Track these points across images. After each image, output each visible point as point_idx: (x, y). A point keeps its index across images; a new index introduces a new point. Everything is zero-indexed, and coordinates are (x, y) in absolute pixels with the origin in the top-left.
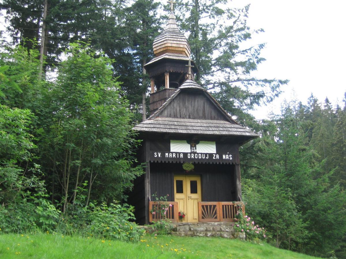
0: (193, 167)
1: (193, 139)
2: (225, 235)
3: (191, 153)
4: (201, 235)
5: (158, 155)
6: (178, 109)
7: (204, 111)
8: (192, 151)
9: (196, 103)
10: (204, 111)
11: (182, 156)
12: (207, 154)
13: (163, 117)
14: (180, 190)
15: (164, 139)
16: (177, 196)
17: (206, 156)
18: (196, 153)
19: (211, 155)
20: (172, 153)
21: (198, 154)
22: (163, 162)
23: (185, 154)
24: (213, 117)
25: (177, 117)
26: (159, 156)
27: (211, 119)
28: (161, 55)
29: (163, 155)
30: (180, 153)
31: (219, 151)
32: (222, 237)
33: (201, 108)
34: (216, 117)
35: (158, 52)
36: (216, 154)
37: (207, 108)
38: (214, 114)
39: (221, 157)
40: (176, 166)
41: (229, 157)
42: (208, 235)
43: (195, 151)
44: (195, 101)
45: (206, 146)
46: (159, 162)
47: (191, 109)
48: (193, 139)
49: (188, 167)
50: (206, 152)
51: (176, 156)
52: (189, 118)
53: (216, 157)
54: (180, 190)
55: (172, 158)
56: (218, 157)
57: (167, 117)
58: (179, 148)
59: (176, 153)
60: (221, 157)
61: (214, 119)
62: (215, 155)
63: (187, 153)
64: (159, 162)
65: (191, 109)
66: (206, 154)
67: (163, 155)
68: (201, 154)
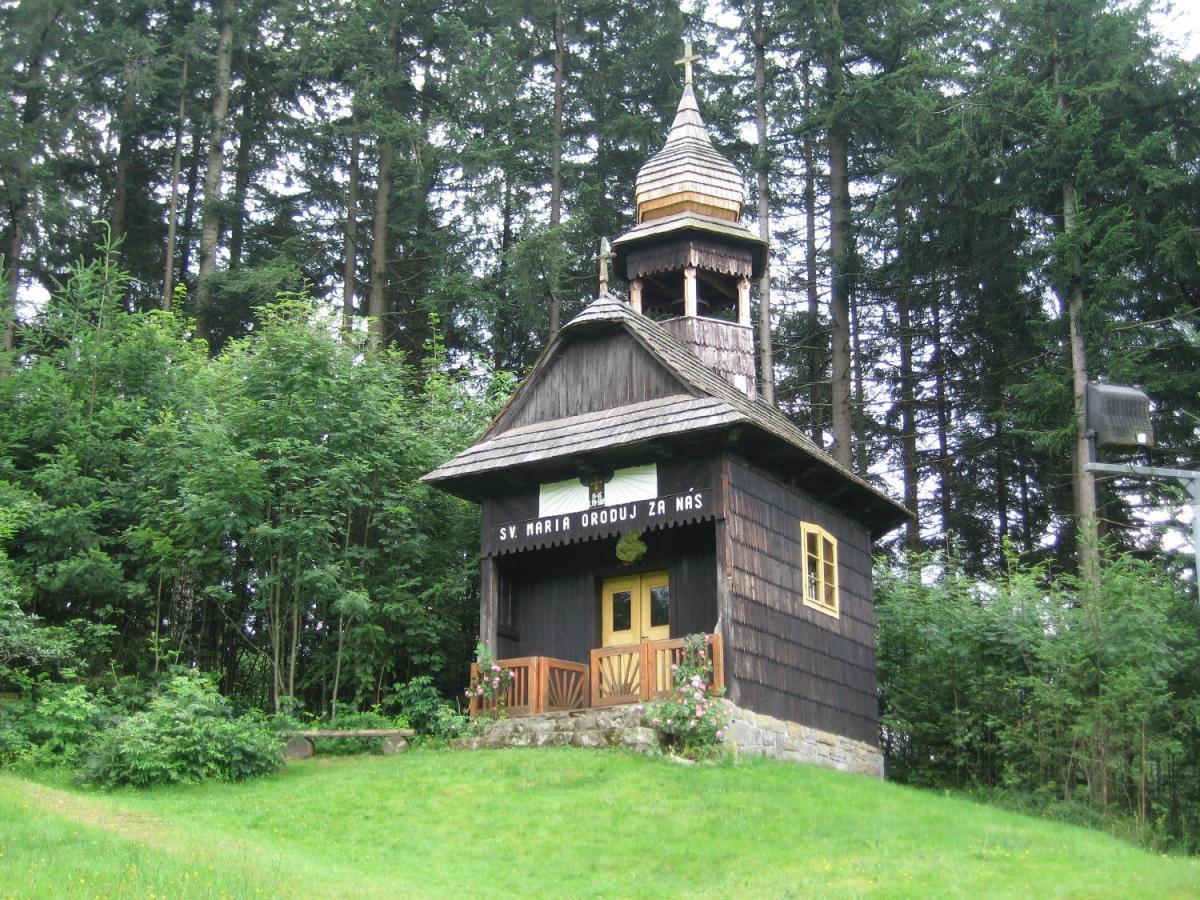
0: (642, 548)
1: (595, 467)
2: (585, 740)
3: (589, 512)
4: (521, 743)
5: (508, 532)
6: (563, 392)
7: (630, 381)
8: (594, 503)
9: (610, 362)
10: (630, 381)
11: (566, 524)
12: (633, 503)
13: (524, 423)
14: (622, 622)
15: (516, 487)
16: (613, 638)
17: (630, 511)
18: (603, 508)
19: (643, 505)
20: (543, 520)
21: (608, 509)
22: (576, 541)
23: (575, 517)
24: (653, 388)
25: (560, 417)
26: (512, 535)
27: (649, 398)
28: (661, 217)
29: (521, 531)
30: (561, 518)
31: (668, 489)
32: (575, 743)
33: (622, 373)
34: (662, 388)
35: (651, 207)
36: (656, 501)
37: (639, 367)
38: (656, 380)
39: (671, 505)
40: (588, 557)
41: (694, 502)
42: (540, 743)
43: (600, 503)
44: (606, 360)
45: (637, 483)
46: (567, 542)
47: (594, 384)
48: (595, 467)
49: (630, 549)
50: (628, 501)
51: (553, 527)
52: (591, 410)
53: (656, 509)
54: (622, 622)
55: (543, 535)
56: (662, 507)
57: (535, 421)
58: (561, 503)
59: (553, 519)
60: (671, 505)
61: (658, 395)
62: (653, 504)
63: (580, 514)
64: (567, 542)
65: (594, 384)
66: (629, 506)
67: (521, 531)
68: (617, 507)
